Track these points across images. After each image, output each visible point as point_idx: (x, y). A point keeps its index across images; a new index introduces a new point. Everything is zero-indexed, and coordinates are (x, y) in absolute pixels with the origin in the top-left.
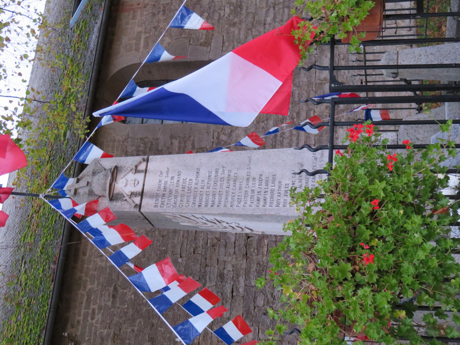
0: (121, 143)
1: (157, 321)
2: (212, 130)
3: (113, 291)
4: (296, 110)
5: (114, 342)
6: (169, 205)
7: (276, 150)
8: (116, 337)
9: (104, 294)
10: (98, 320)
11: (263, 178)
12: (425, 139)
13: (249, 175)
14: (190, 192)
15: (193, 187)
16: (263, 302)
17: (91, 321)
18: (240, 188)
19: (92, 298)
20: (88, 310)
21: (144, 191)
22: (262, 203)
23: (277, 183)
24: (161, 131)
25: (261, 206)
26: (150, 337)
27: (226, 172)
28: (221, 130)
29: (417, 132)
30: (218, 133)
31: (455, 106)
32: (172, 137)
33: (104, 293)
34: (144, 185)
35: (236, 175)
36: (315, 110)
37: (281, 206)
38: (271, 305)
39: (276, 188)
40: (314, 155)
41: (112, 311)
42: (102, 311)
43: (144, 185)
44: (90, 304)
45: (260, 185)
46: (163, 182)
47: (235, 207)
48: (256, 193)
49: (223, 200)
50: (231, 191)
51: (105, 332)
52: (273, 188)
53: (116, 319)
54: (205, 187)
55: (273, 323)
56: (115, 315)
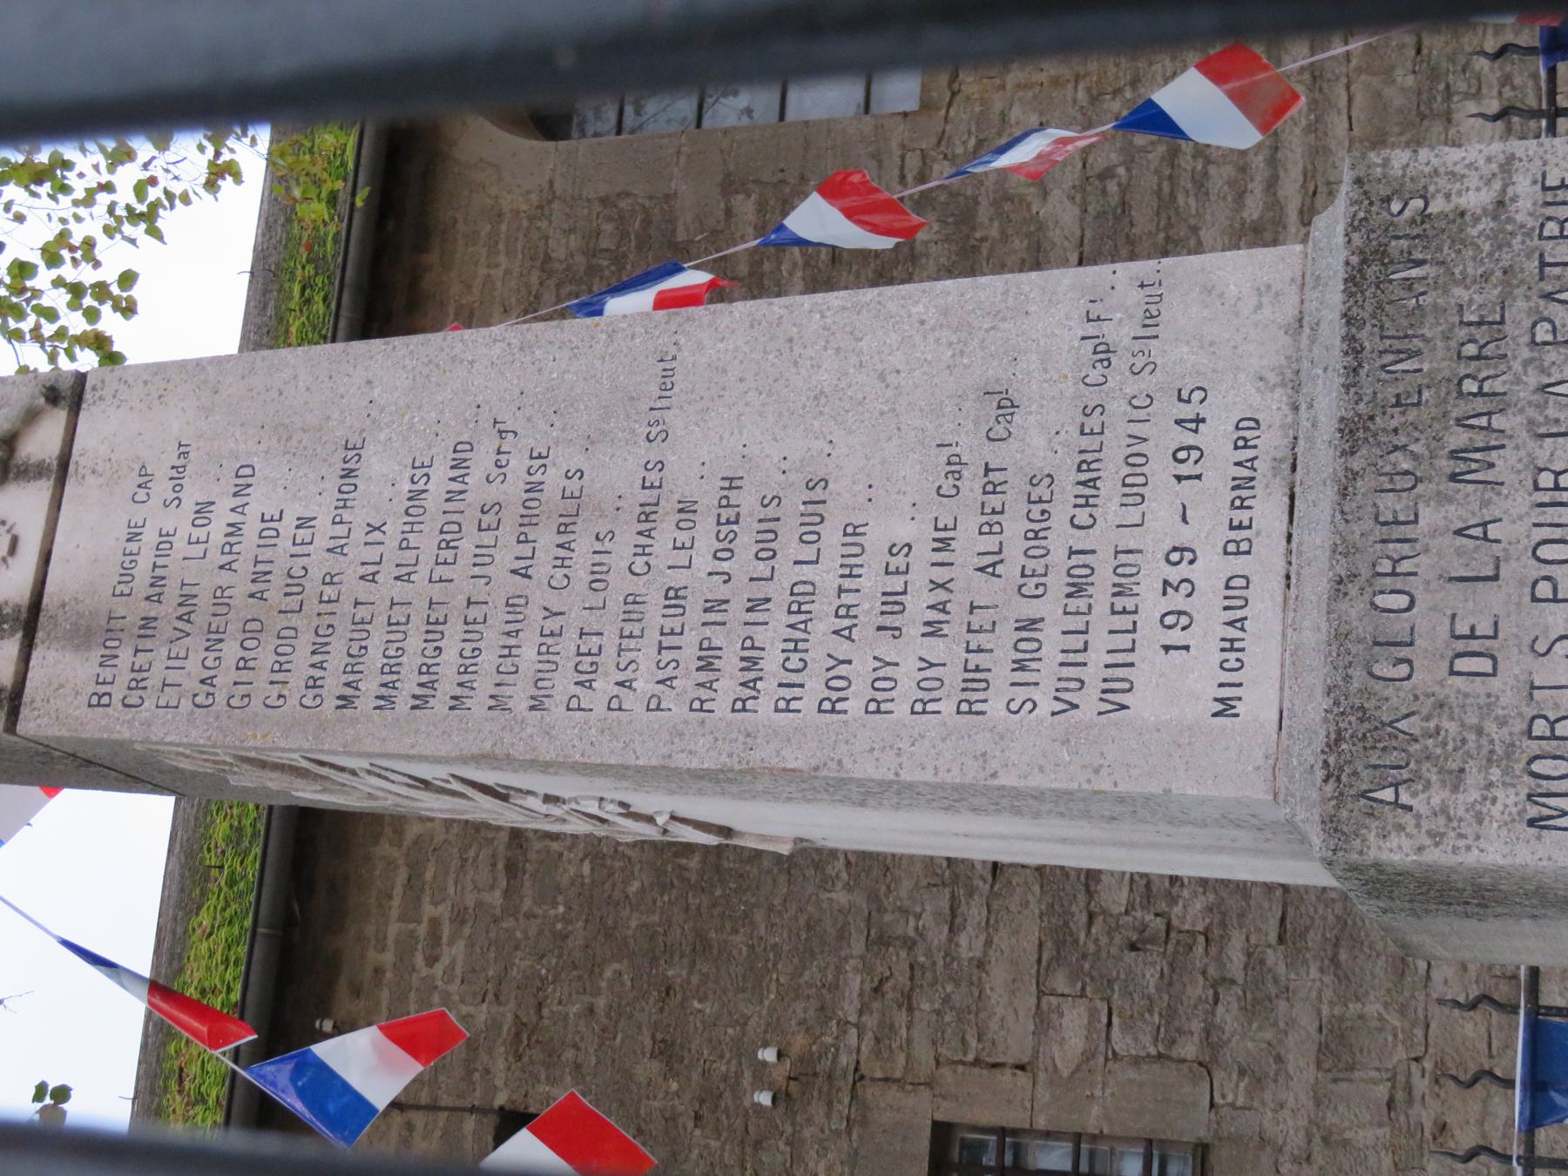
0: (525, 223)
1: (684, 973)
2: (894, 144)
3: (509, 846)
5: (519, 1058)
6: (170, 695)
7: (835, 299)
8: (525, 1036)
9: (475, 859)
10: (452, 967)
11: (747, 500)
13: (653, 479)
14: (292, 603)
15: (316, 574)
16: (1125, 892)
17: (424, 972)
18: (597, 581)
19: (429, 875)
20: (411, 926)
21: (45, 601)
22: (728, 686)
23: (832, 536)
24: (683, 160)
25: (722, 706)
26: (659, 1036)
27: (518, 465)
28: (934, 140)
30: (924, 156)
32: (730, 186)
33: (472, 853)
34: (46, 557)
35: (574, 485)
37: (854, 706)
38: (1162, 906)
39: (827, 576)
40: (1091, 329)
41: (507, 930)
42: (467, 931)
43: (46, 557)
44: (419, 899)
45: (724, 552)
46: (150, 537)
47: (557, 710)
48: (695, 614)
49: (488, 660)
50: (539, 596)
51: (482, 1013)
52: (807, 572)
53: (522, 963)
54: (387, 572)
55: (1170, 984)
56: (517, 948)
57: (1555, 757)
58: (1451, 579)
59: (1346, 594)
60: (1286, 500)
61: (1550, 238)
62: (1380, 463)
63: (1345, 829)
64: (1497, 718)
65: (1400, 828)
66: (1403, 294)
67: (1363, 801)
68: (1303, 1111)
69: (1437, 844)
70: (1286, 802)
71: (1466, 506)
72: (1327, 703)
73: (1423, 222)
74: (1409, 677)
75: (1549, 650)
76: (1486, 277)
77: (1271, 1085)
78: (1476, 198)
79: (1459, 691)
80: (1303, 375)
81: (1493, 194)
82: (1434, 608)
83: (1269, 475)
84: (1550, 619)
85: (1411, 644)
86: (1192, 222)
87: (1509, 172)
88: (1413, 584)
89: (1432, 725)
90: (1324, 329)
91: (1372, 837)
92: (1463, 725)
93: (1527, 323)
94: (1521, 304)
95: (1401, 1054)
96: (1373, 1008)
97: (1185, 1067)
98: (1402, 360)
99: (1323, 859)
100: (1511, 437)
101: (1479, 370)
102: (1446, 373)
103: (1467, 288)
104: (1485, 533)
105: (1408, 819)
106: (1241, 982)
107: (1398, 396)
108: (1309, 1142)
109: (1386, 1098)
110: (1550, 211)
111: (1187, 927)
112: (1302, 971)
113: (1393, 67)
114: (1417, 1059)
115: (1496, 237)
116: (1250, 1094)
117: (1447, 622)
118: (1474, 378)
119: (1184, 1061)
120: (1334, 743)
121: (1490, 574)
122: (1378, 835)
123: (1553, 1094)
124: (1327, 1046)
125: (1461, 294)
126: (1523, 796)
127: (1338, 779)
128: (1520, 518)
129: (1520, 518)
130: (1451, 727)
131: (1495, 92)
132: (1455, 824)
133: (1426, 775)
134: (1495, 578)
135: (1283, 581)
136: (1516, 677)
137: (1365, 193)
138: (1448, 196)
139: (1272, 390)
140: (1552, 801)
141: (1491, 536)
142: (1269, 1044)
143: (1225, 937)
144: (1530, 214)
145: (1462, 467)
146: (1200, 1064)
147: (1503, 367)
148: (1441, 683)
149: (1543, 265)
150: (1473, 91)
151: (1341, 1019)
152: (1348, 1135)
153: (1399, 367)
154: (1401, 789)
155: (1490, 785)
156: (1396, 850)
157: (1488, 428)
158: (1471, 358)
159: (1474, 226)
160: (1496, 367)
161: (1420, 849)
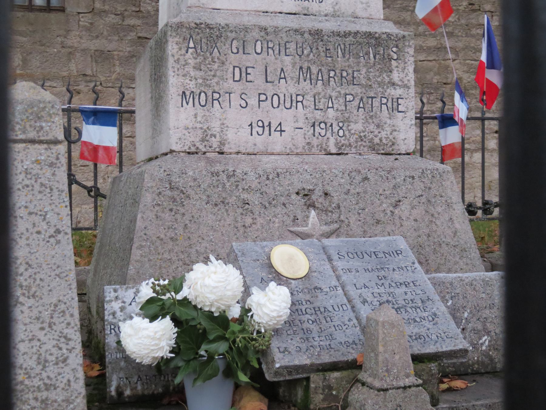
4: (457, 32)
12: (397, 222)
29: (415, 202)
31: (484, 295)
36: (457, 61)
57: (206, 100)
58: (266, 67)
59: (261, 31)
60: (294, 12)
61: (381, 100)
62: (306, 43)
63: (179, 30)
64: (219, 81)
65: (180, 49)
66: (364, 52)
67: (189, 36)
68: (80, 45)
69: (175, 61)
70: (188, 10)
71: (291, 72)
72: (223, 24)
73: (389, 58)
74: (232, 52)
75: (243, 99)
76: (369, 79)
77: (88, 34)
78: (396, 76)
79: (228, 69)
80: (338, 18)
81: (397, 82)
82: (256, 61)
83: (303, 6)
84: (253, 99)
85: (244, 53)
86: (392, 6)
87: (404, 87)
88: (264, 54)
89: (216, 60)
90: (353, 25)
91: (176, 39)
92: (216, 70)
93: (353, 92)
94: (360, 91)
95: (103, 79)
96: (118, 69)
97: (92, 3)
98: (342, 51)
99: (168, 22)
100: (314, 87)
101: (337, 77)
102: (337, 66)
103: (366, 73)
104: (282, 78)
105: (183, 52)
106: (124, 24)
107: (329, 50)
108: (69, 47)
109: (87, 74)
110: (390, 100)
111: (142, 4)
112: (129, 45)
113: (440, 75)
114: (101, 84)
115: (382, 83)
116: (84, 26)
117: (252, 66)
118: (335, 75)
119: (94, 3)
120: (208, 26)
121: (268, 80)
122: (177, 41)
123: (93, 118)
124: (103, 53)
125: (364, 71)
126: (193, 90)
127: (196, 28)
128: (287, 90)
129: (287, 90)
130: (216, 66)
131: (429, 109)
132: (182, 67)
133: (199, 58)
134: (267, 82)
135: (265, 11)
136: (233, 88)
137: (400, 39)
138: (397, 67)
139: (333, 8)
140: (191, 99)
141: (281, 80)
142: (102, 33)
143: (139, 18)
144: (389, 94)
145: (305, 71)
146: (93, 9)
147: (338, 85)
148: (231, 63)
149: (372, 98)
150: (430, 102)
151: (113, 58)
152: (73, 61)
153: (339, 50)
154: (193, 50)
155: (196, 79)
156: (172, 47)
157: (318, 80)
158: (341, 74)
159: (386, 75)
160: (338, 82)
161: (173, 56)
